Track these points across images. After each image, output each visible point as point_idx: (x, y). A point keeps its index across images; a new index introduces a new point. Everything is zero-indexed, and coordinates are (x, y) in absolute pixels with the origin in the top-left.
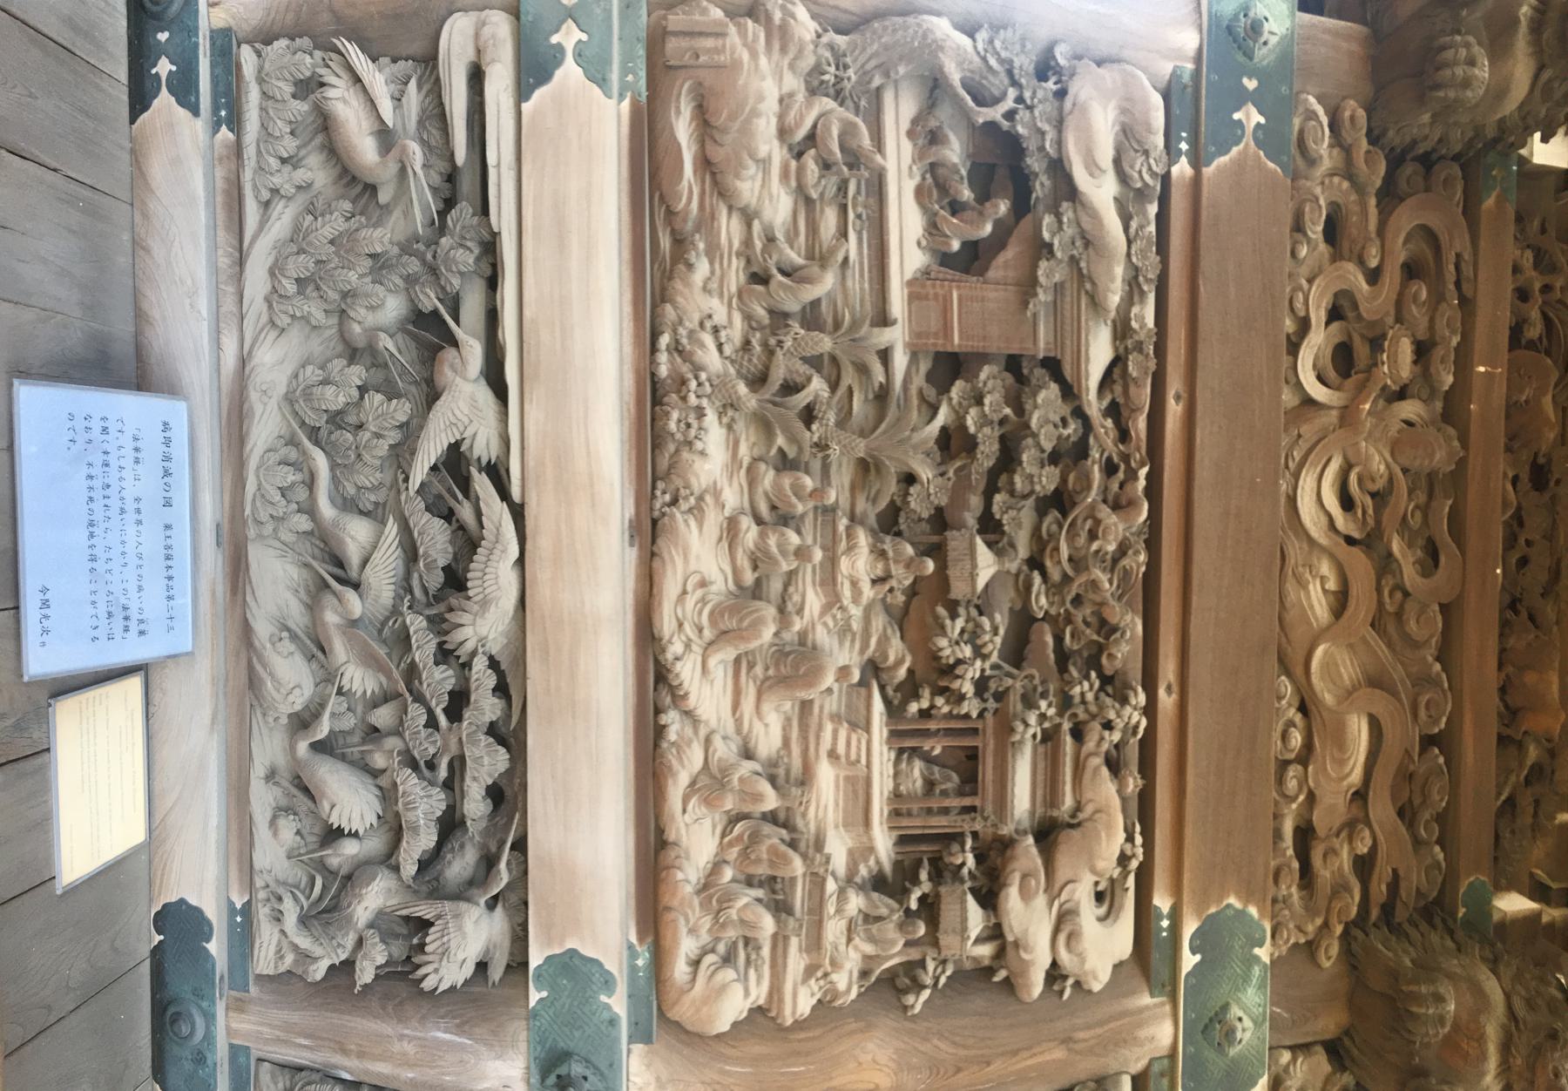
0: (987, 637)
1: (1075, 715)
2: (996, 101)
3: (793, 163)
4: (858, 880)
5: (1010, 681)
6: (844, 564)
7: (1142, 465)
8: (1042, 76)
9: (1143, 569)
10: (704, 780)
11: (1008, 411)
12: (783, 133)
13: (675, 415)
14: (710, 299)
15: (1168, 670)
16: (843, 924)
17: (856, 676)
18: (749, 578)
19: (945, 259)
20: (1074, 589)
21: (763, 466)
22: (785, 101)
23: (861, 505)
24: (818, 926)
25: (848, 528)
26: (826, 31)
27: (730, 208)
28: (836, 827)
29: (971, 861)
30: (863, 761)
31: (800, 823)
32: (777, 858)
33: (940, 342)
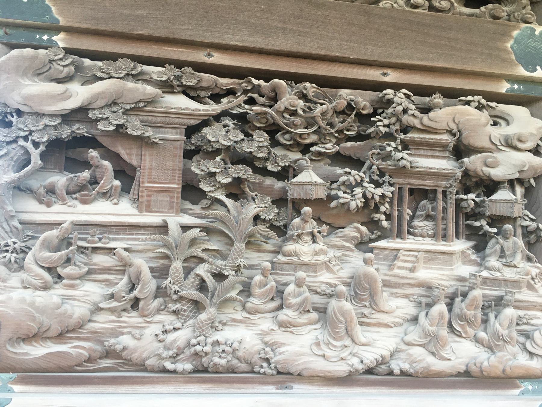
0: (352, 179)
1: (396, 130)
2: (27, 152)
3: (65, 281)
4: (479, 260)
5: (374, 167)
6: (306, 258)
7: (250, 82)
8: (9, 125)
9: (314, 85)
10: (432, 348)
11: (218, 159)
12: (46, 287)
13: (216, 360)
14: (146, 335)
15: (373, 74)
16: (506, 269)
18: (314, 315)
19: (126, 189)
21: (248, 305)
24: (508, 282)
25: (284, 255)
27: (90, 321)
28: (452, 269)
29: (472, 196)
30: (416, 253)
31: (451, 290)
32: (473, 305)
33: (176, 195)
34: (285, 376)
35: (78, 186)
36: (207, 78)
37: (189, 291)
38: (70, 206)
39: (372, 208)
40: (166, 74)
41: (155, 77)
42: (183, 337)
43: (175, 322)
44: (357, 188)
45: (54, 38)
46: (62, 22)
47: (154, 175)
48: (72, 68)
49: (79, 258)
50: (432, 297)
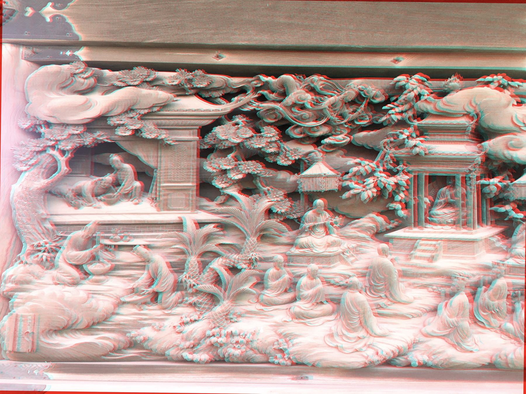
1: (409, 118)
2: (55, 161)
5: (388, 157)
6: (319, 250)
7: (259, 79)
8: (38, 135)
11: (230, 156)
12: (74, 283)
17: (384, 245)
18: (328, 307)
19: (146, 189)
20: (333, 117)
21: (262, 297)
22: (57, 282)
23: (283, 239)
25: (297, 248)
26: (19, 258)
27: (113, 314)
28: (474, 258)
29: (495, 181)
31: (473, 280)
32: (498, 295)
33: (191, 193)
34: (300, 367)
35: (103, 188)
36: (218, 79)
37: (204, 285)
38: (95, 208)
39: (387, 198)
40: (177, 79)
41: (167, 82)
42: (199, 329)
43: (191, 314)
44: (368, 178)
45: (77, 53)
46: (82, 37)
47: (170, 175)
48: (92, 80)
49: (104, 255)
50: (451, 287)
